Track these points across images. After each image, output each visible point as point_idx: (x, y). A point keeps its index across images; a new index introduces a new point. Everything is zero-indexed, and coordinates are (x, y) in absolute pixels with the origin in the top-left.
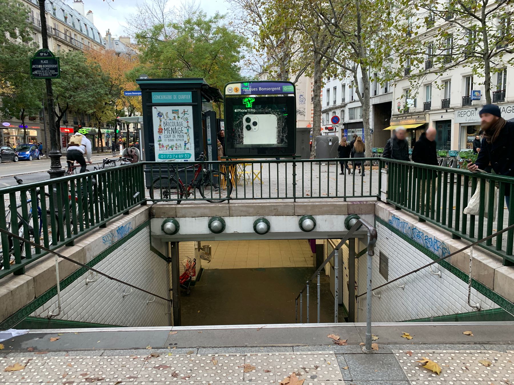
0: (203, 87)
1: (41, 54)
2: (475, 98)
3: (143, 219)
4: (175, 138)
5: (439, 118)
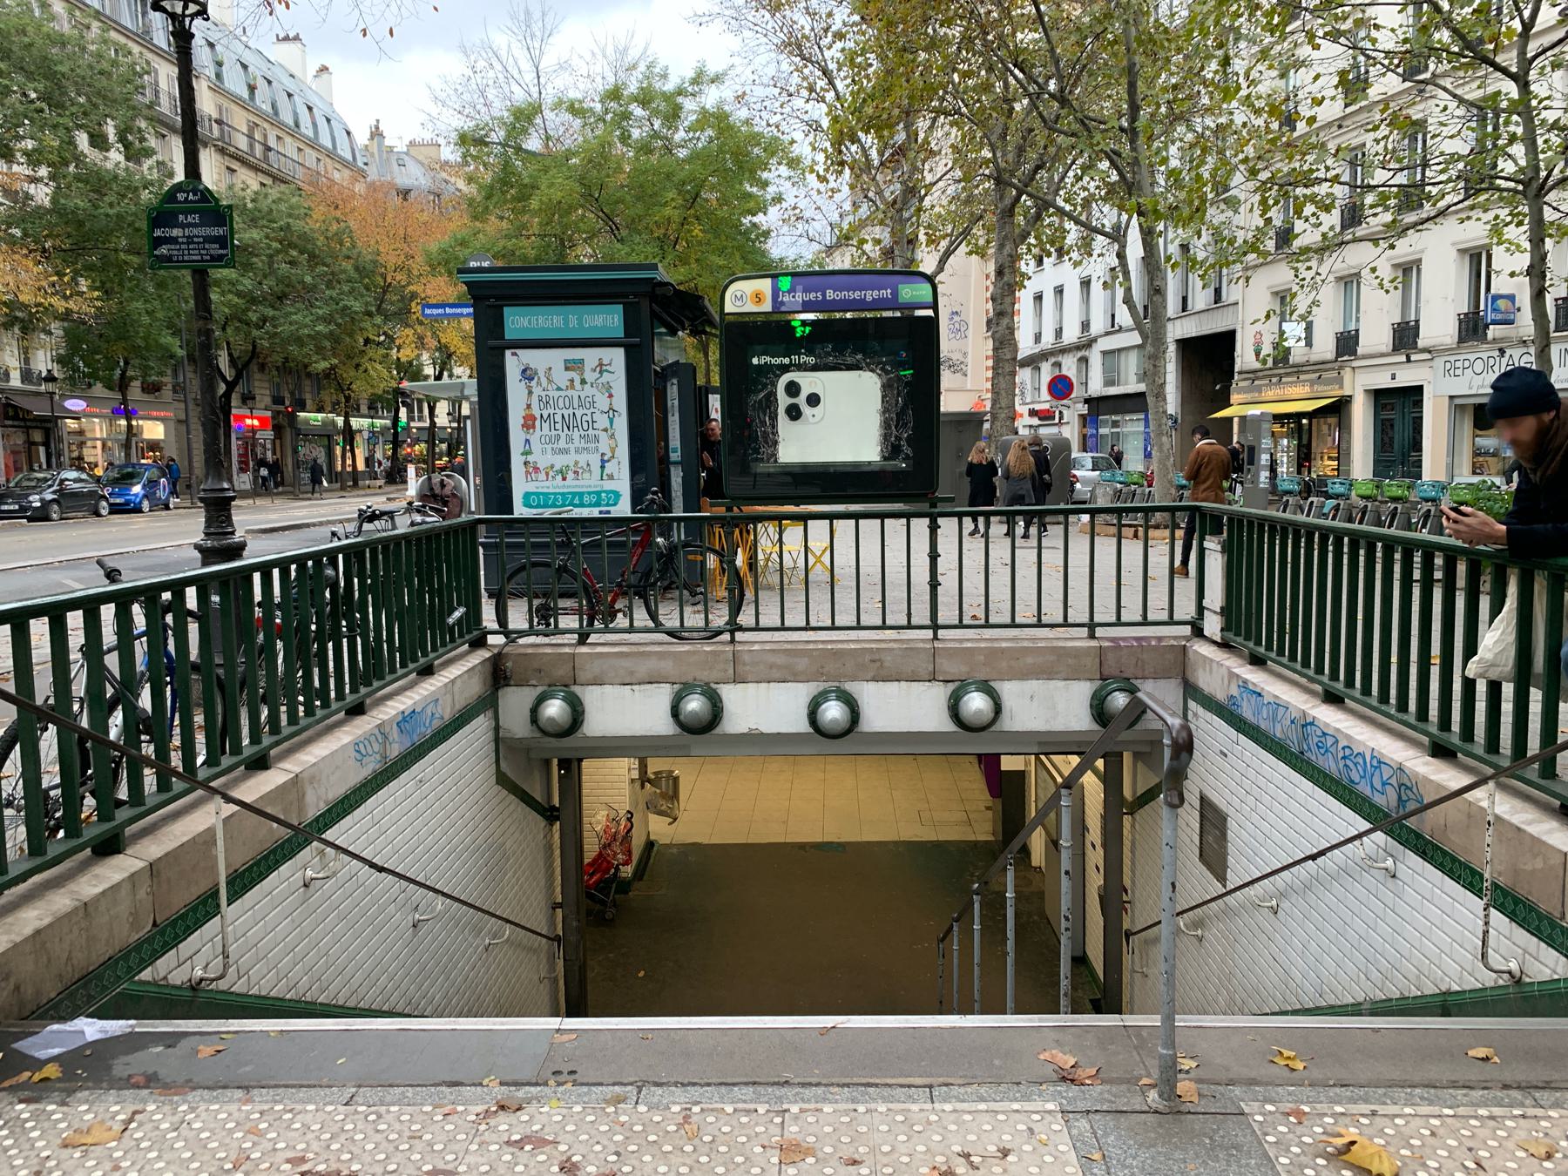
0: (658, 291)
1: (181, 196)
2: (1499, 317)
4: (574, 445)
5: (1383, 381)
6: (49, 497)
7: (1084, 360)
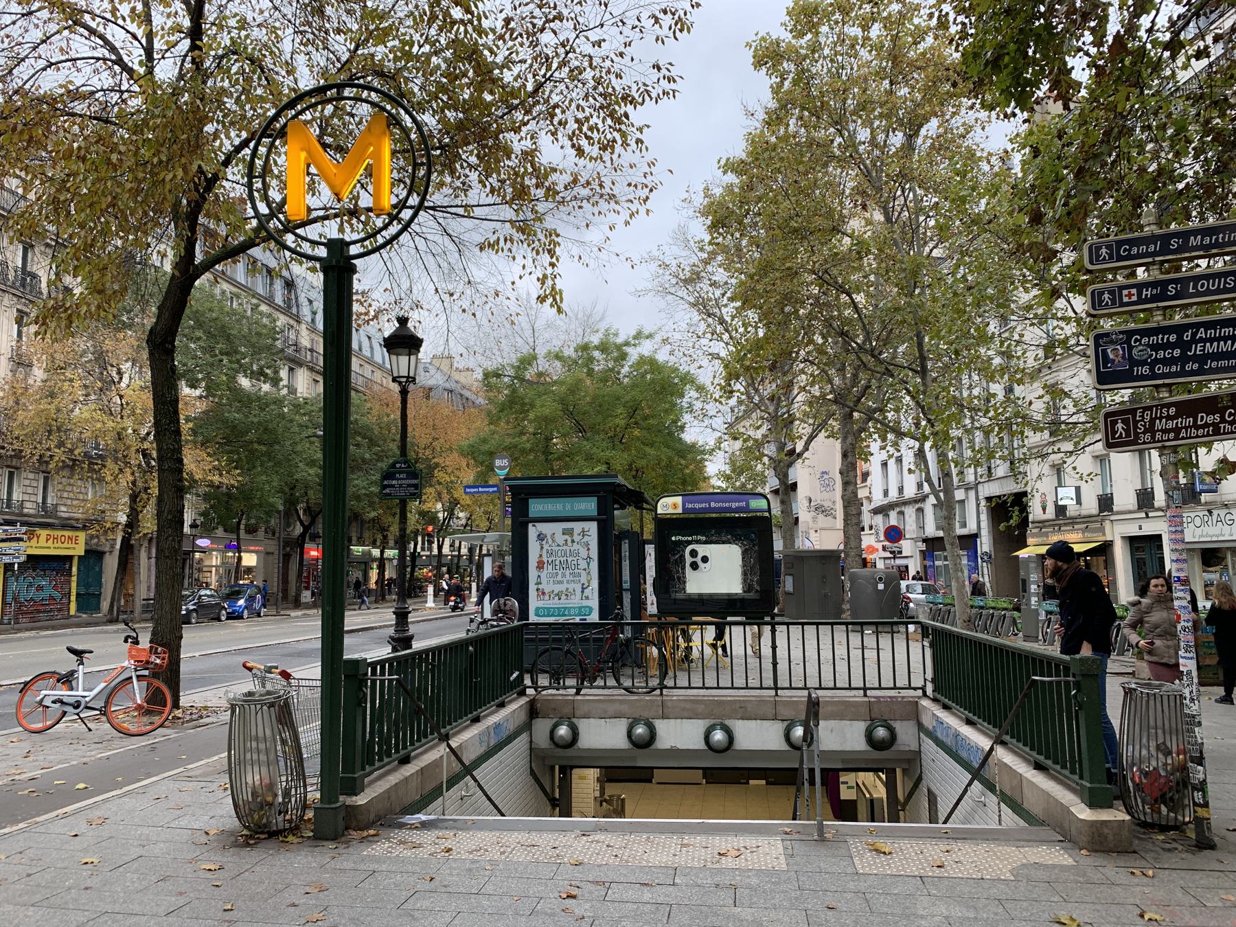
0: (618, 490)
2: (1205, 487)
3: (522, 717)
4: (566, 580)
5: (1133, 530)
6: (192, 608)
7: (920, 510)
